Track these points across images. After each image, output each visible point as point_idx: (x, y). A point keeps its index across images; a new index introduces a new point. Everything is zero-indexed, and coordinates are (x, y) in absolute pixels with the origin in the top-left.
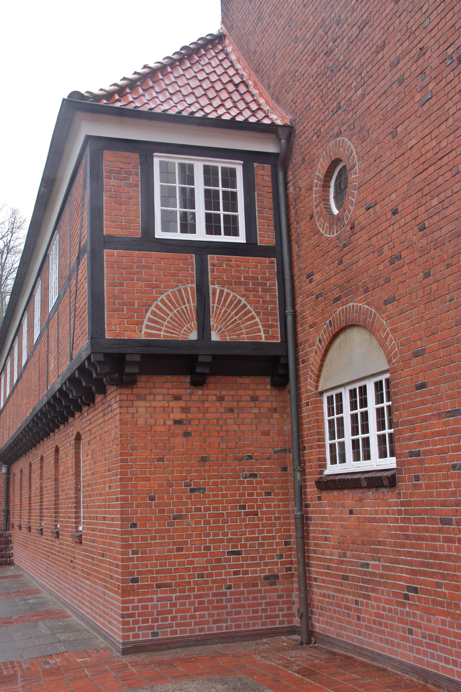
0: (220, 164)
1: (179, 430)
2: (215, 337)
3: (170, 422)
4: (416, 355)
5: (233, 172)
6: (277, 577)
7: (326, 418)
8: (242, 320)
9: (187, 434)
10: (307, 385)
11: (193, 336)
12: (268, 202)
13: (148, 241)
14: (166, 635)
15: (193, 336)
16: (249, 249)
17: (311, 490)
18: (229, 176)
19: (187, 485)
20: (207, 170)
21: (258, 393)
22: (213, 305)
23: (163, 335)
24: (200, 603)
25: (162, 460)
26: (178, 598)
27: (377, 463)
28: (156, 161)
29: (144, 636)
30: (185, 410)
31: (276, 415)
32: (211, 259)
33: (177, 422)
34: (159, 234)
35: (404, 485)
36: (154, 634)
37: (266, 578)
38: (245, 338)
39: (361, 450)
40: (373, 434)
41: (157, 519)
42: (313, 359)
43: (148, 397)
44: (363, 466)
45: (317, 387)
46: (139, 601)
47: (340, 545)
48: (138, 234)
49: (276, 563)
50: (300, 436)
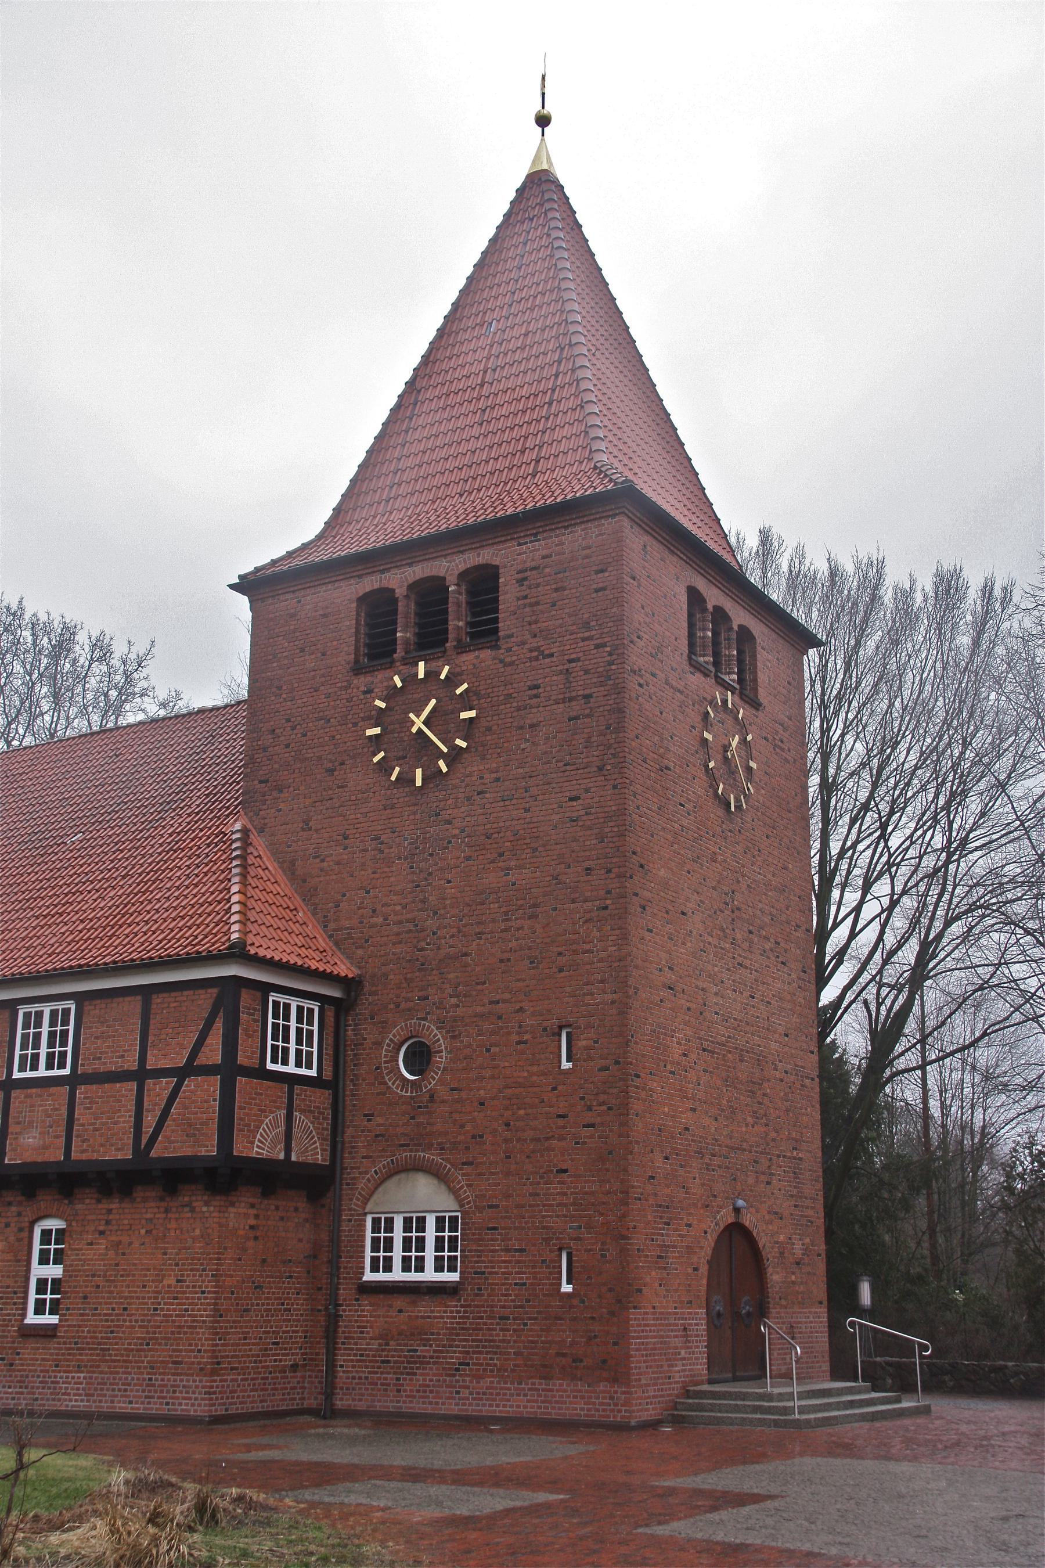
1: (251, 1234)
2: (294, 1158)
3: (247, 1227)
4: (490, 1207)
5: (311, 1011)
6: (297, 1365)
9: (256, 1238)
11: (282, 1156)
15: (282, 1156)
17: (345, 1292)
19: (253, 1282)
20: (300, 1009)
21: (299, 1204)
24: (254, 1385)
25: (240, 1260)
26: (242, 1380)
29: (221, 1411)
30: (257, 1217)
31: (307, 1225)
33: (252, 1227)
36: (226, 1410)
37: (292, 1366)
38: (310, 1159)
41: (236, 1310)
43: (237, 1204)
45: (364, 1209)
46: (221, 1381)
49: (297, 1354)
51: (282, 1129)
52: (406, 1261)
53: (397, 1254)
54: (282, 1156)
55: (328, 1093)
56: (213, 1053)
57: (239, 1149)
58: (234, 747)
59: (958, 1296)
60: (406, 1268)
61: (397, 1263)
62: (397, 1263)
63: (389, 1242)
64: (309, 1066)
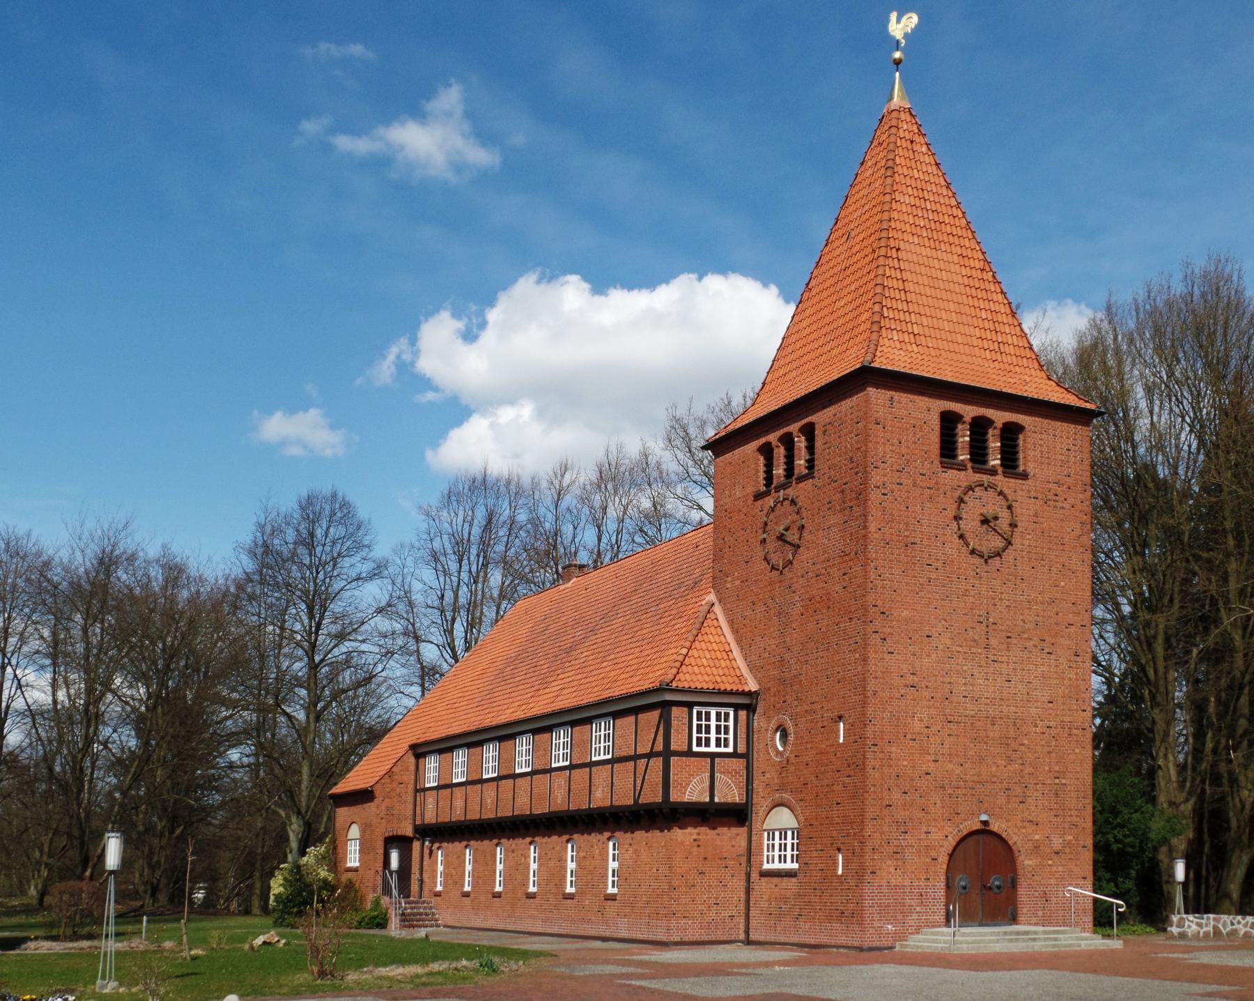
0: (723, 710)
2: (716, 800)
7: (766, 842)
8: (729, 792)
10: (756, 825)
11: (707, 800)
12: (744, 730)
13: (689, 753)
14: (686, 939)
16: (735, 755)
18: (727, 715)
22: (717, 784)
23: (694, 799)
27: (791, 865)
28: (695, 712)
32: (717, 760)
34: (695, 749)
35: (800, 876)
38: (730, 800)
39: (782, 859)
40: (789, 853)
42: (761, 814)
44: (782, 866)
47: (769, 900)
48: (686, 748)
50: (750, 849)
51: (707, 783)
52: (718, 740)
53: (713, 736)
54: (707, 800)
55: (743, 761)
56: (659, 746)
57: (675, 797)
58: (706, 538)
59: (1202, 528)
60: (718, 745)
61: (713, 742)
62: (713, 742)
63: (708, 727)
64: (726, 746)
